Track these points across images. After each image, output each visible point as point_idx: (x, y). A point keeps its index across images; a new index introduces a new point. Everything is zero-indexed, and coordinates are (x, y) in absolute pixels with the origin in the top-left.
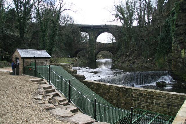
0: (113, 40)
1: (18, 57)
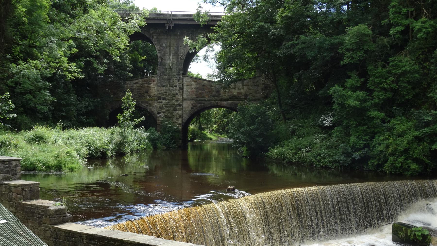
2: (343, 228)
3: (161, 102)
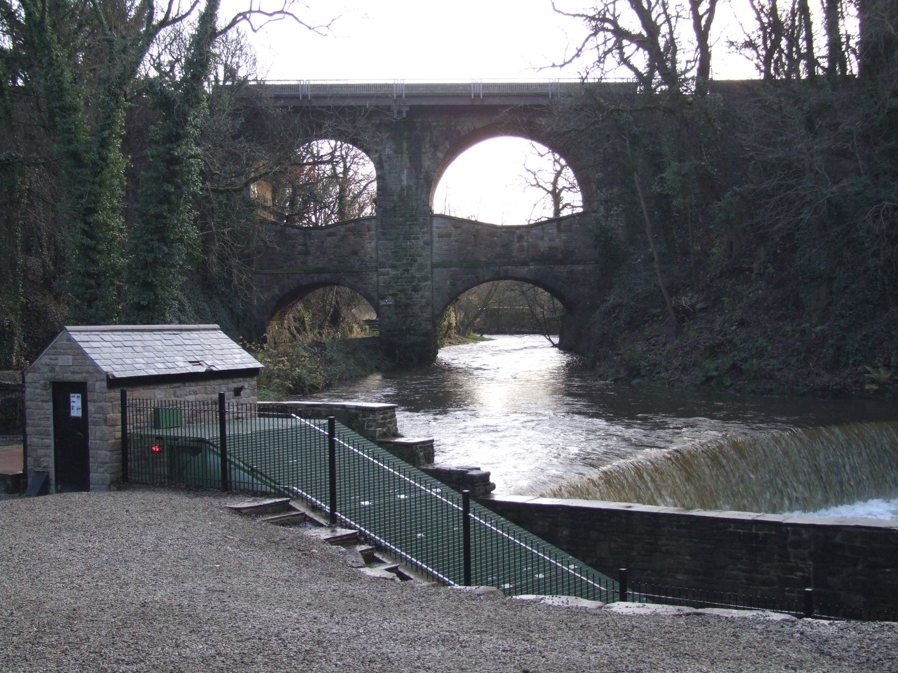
0: (556, 196)
1: (78, 378)
2: (507, 246)
3: (388, 274)
